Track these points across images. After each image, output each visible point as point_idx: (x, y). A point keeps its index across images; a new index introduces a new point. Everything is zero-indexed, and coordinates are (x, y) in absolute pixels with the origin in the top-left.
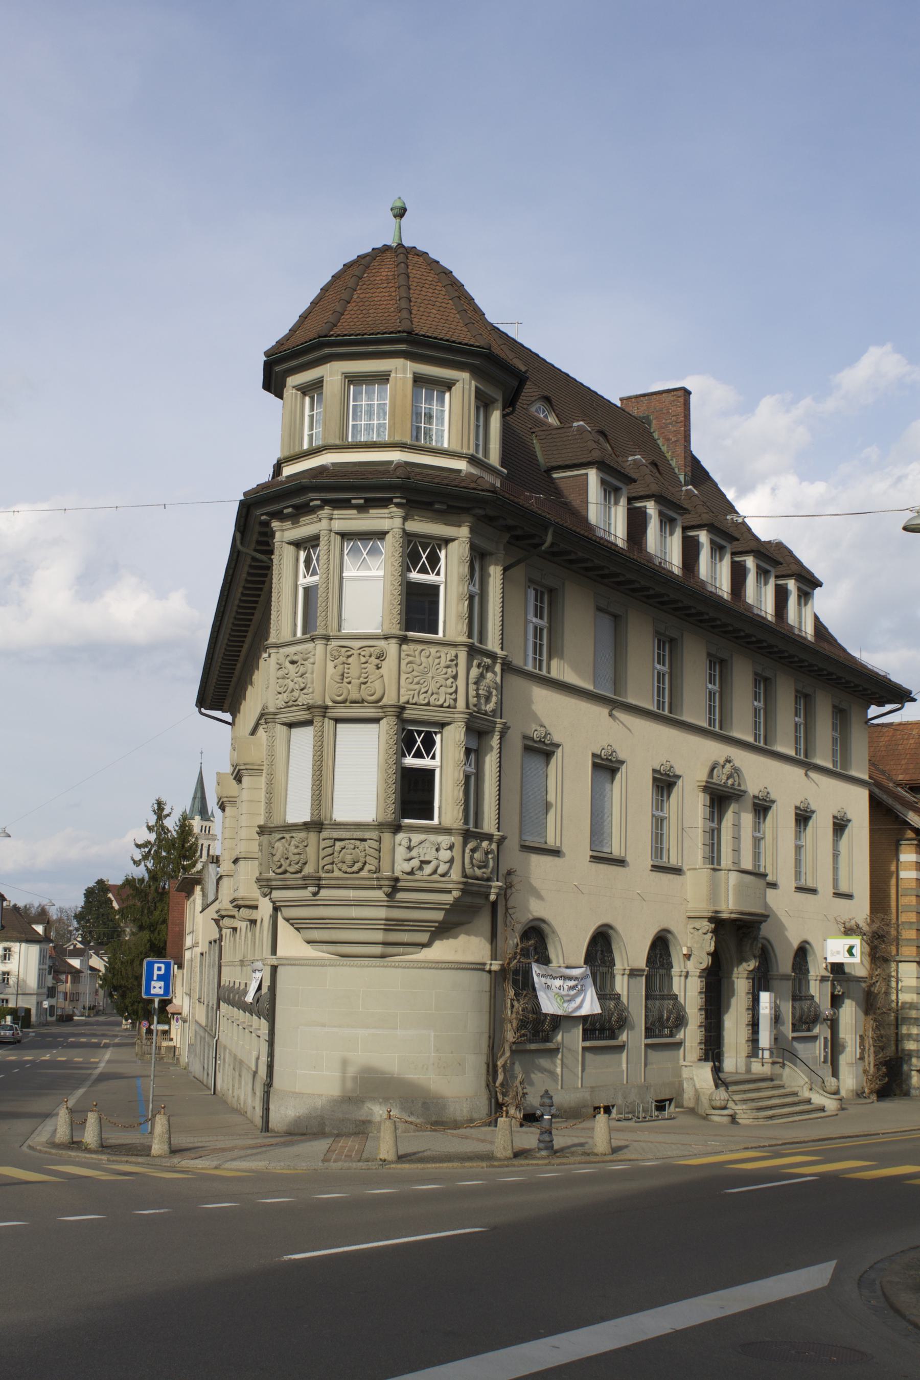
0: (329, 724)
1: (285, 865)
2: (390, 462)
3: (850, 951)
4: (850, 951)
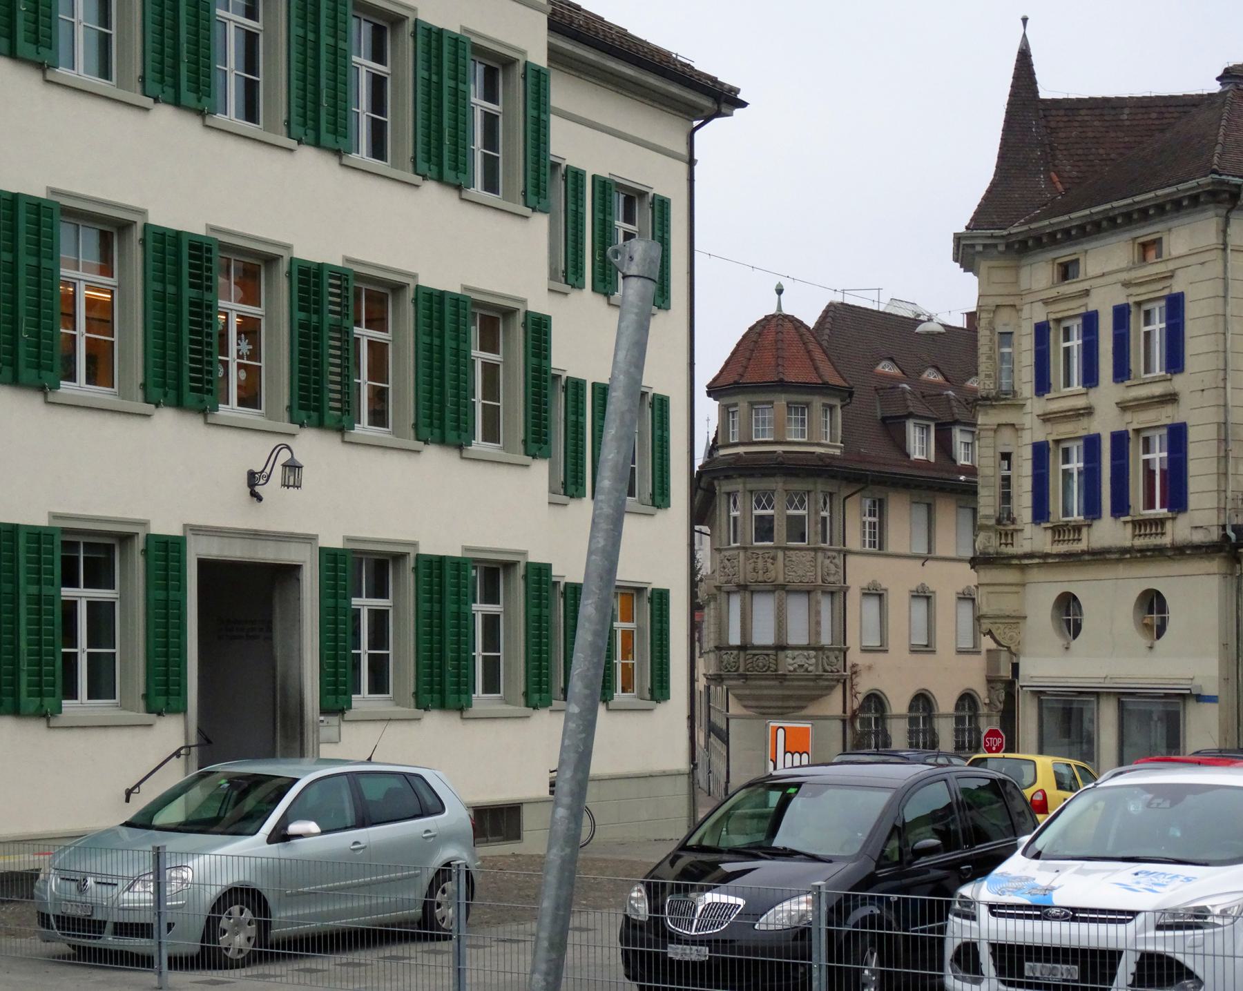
0: (748, 595)
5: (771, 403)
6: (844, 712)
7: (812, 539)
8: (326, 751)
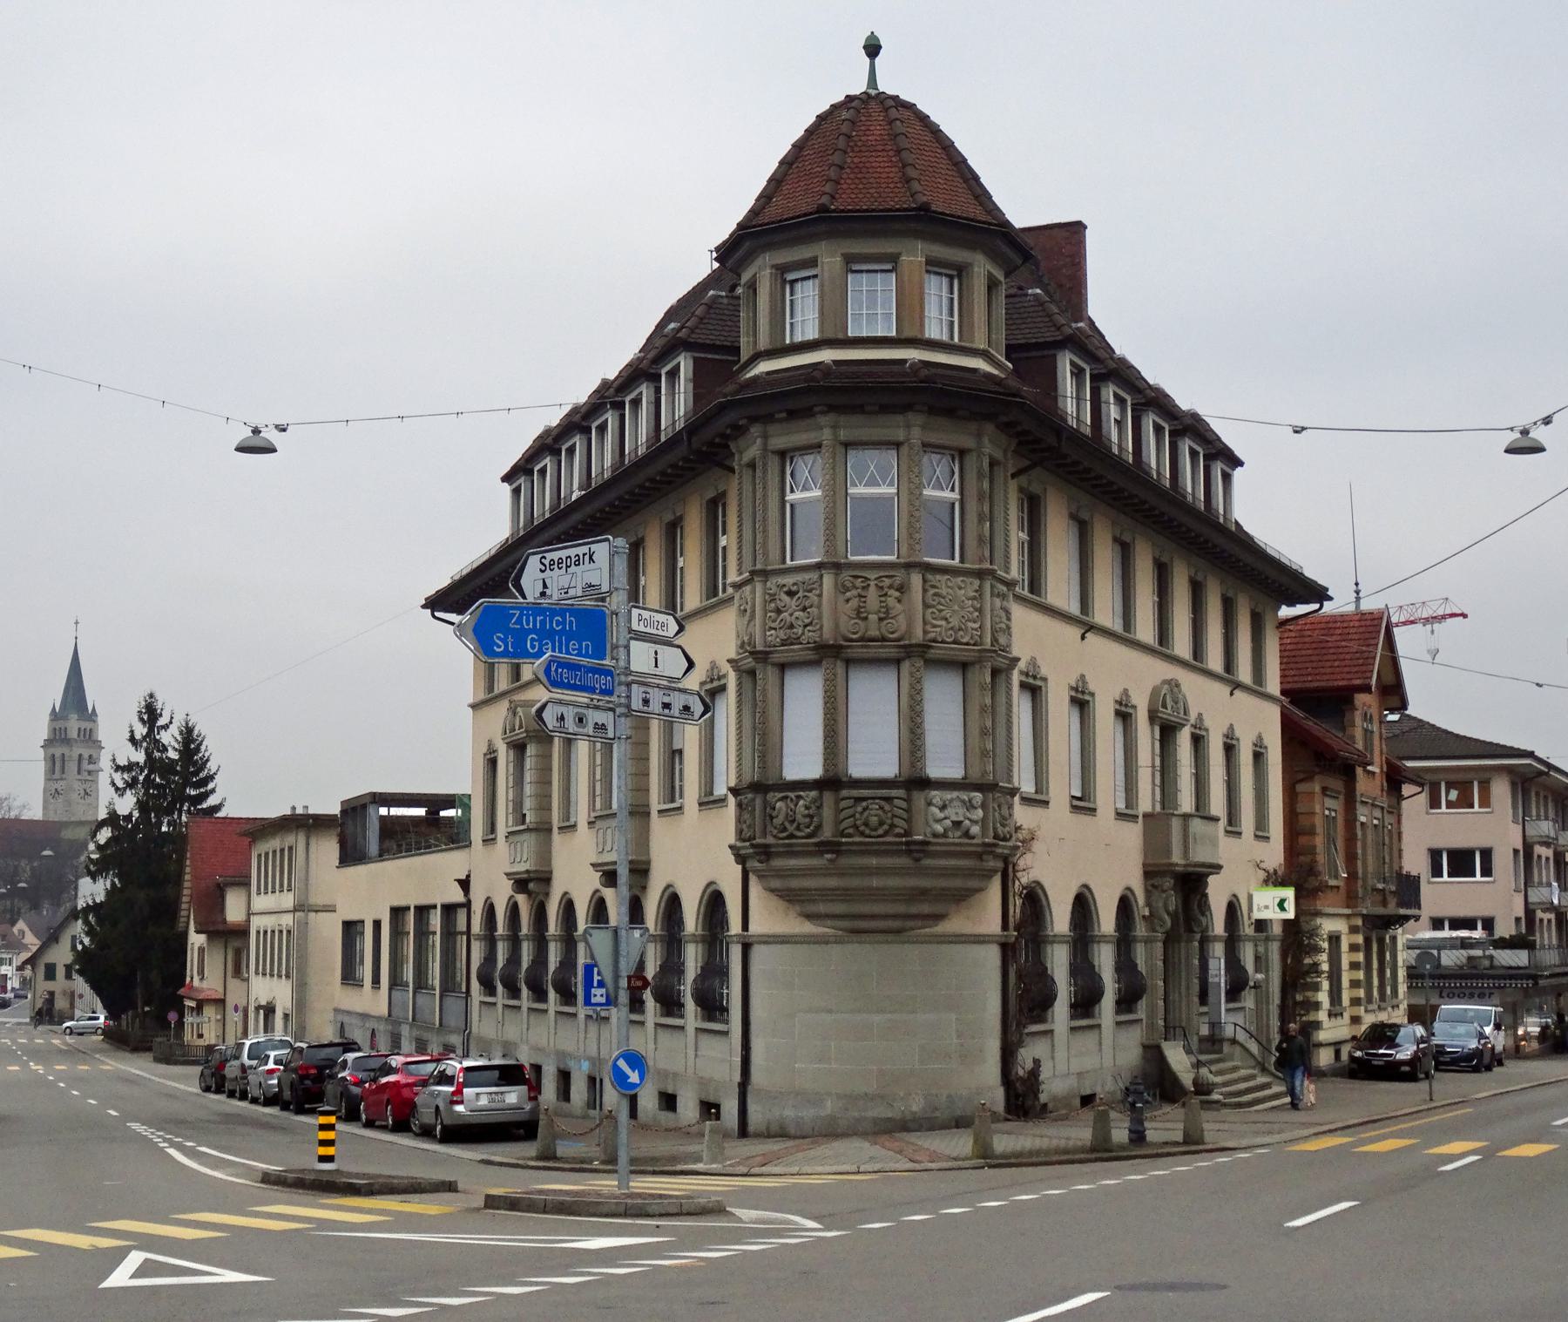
0: (840, 668)
1: (791, 828)
2: (904, 361)
3: (1281, 905)
4: (1281, 905)
5: (894, 259)
6: (1005, 926)
7: (969, 553)
8: (1306, 1082)
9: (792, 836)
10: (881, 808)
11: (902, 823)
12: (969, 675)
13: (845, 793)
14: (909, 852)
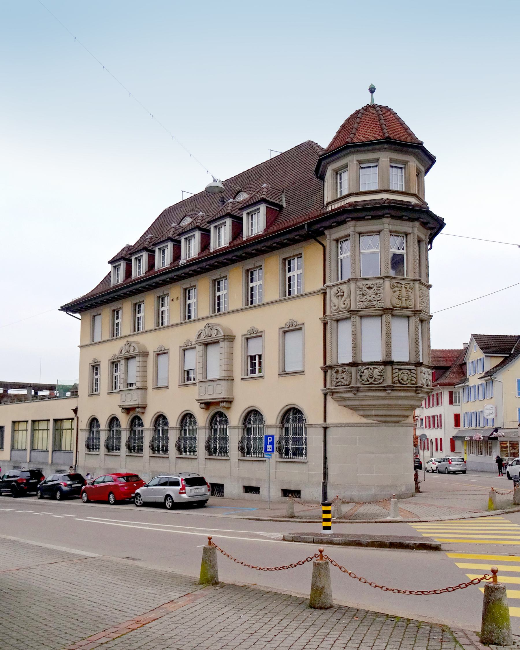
5: (377, 160)
9: (371, 383)
10: (407, 373)
11: (415, 379)
12: (424, 325)
13: (395, 367)
14: (416, 391)
